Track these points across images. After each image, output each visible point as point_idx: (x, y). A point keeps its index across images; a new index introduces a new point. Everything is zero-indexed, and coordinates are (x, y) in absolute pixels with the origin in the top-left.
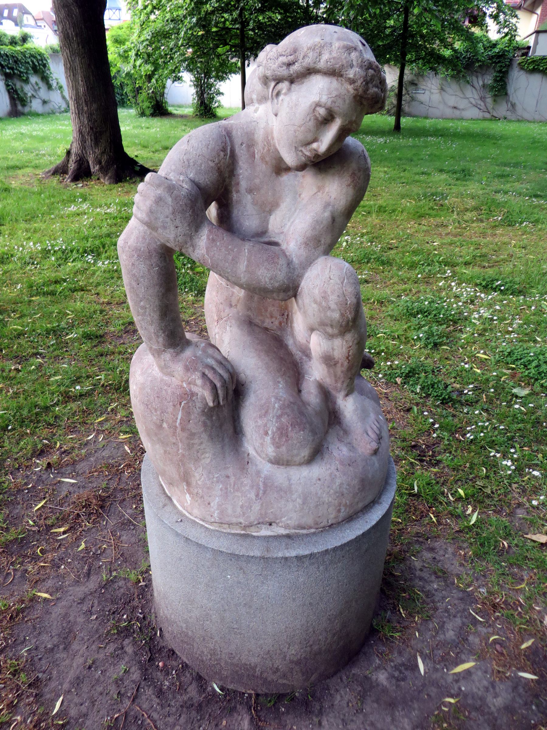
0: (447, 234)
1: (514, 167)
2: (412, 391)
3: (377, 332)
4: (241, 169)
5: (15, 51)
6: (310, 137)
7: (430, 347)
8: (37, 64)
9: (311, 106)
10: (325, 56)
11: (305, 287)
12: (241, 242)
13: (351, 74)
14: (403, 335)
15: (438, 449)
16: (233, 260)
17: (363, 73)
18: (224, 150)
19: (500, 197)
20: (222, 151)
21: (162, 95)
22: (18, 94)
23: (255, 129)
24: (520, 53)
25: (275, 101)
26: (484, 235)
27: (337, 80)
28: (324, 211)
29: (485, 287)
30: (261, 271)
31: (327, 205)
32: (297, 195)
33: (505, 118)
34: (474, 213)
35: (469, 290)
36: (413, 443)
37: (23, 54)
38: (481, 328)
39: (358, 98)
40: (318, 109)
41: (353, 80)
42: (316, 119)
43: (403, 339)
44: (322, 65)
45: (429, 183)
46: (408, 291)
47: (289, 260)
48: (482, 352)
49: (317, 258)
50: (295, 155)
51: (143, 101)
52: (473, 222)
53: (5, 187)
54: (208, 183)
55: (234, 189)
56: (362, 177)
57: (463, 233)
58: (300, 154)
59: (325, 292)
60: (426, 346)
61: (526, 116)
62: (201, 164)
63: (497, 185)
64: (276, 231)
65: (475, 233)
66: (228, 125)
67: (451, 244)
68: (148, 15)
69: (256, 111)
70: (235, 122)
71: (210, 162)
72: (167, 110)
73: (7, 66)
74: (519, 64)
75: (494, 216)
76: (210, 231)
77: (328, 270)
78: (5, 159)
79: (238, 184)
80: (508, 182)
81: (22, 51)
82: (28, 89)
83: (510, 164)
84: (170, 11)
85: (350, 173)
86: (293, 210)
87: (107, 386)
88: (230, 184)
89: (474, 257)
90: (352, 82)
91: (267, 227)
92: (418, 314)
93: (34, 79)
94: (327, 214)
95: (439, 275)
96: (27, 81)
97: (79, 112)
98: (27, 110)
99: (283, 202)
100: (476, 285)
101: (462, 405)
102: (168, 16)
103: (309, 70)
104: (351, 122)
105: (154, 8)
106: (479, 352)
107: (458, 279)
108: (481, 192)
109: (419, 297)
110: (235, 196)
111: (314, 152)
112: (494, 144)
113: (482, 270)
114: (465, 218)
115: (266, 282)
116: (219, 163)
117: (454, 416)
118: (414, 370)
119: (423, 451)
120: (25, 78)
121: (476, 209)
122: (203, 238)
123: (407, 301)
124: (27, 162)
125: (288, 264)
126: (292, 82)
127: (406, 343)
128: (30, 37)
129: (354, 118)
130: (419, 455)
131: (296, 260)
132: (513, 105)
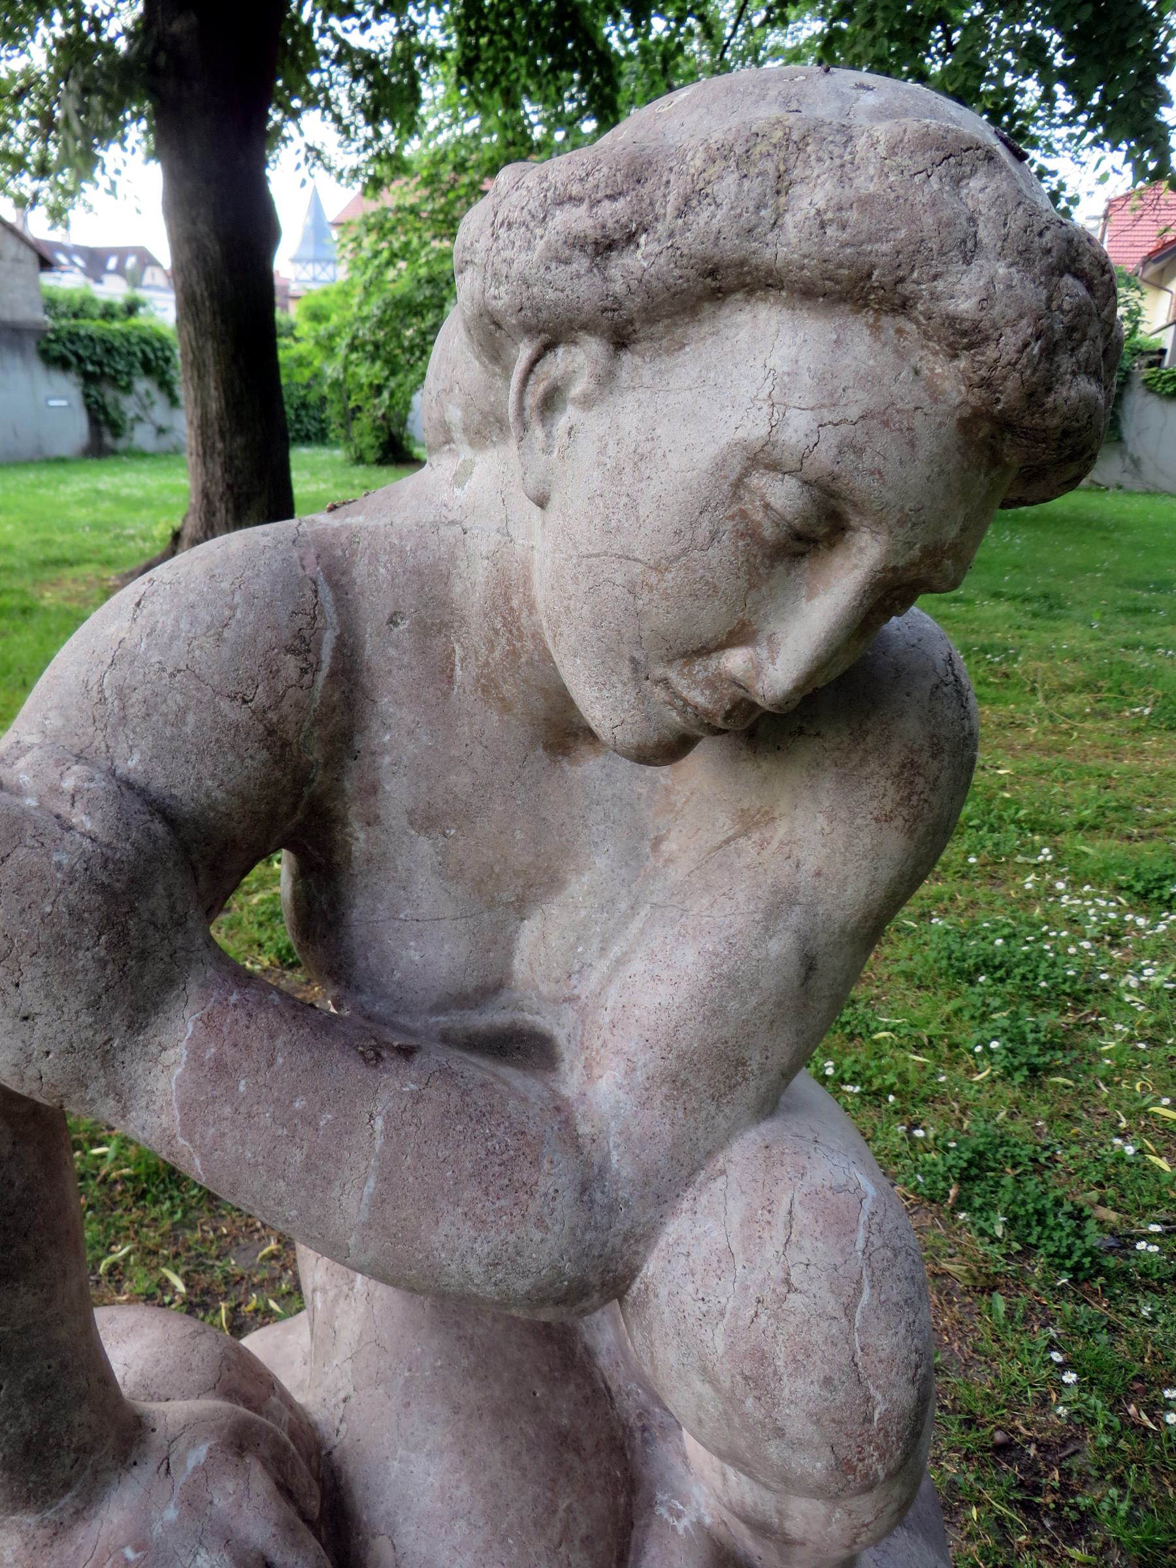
0: (1028, 747)
1: (1157, 590)
2: (982, 1233)
3: (873, 1025)
4: (387, 727)
5: (110, 331)
6: (710, 620)
7: (1019, 1078)
8: (152, 356)
9: (720, 465)
10: (813, 195)
11: (663, 1292)
12: (359, 1071)
13: (963, 293)
14: (942, 1037)
15: (1076, 1463)
16: (309, 1166)
17: (1032, 294)
18: (303, 646)
19: (1139, 660)
20: (290, 650)
21: (403, 422)
22: (106, 413)
23: (453, 558)
24: (1144, 362)
25: (538, 432)
26: (1116, 753)
27: (875, 329)
28: (768, 932)
29: (1144, 895)
30: (445, 1228)
31: (781, 901)
32: (640, 846)
33: (1120, 487)
34: (1086, 697)
35: (1103, 903)
36: (999, 1436)
37: (126, 337)
38: (1151, 1020)
39: (985, 429)
40: (757, 480)
41: (976, 327)
42: (750, 533)
43: (943, 1047)
44: (789, 243)
45: (971, 621)
46: (946, 902)
47: (588, 1164)
48: (1166, 1101)
49: (722, 1144)
50: (631, 696)
51: (361, 435)
52: (1085, 717)
53: (27, 603)
54: (219, 794)
55: (354, 812)
56: (944, 777)
57: (1065, 745)
58: (660, 694)
59: (761, 1357)
60: (1009, 1072)
61: (1164, 483)
62: (183, 711)
63: (1125, 629)
64: (544, 989)
65: (1094, 746)
66: (337, 532)
67: (1039, 774)
68: (381, 270)
69: (460, 477)
70: (371, 524)
71: (225, 705)
72: (410, 453)
73: (90, 358)
74: (1145, 381)
75: (1131, 705)
76: (208, 1022)
77: (780, 1234)
78: (47, 542)
79: (373, 789)
80: (1149, 624)
81: (125, 330)
82: (129, 406)
83: (1147, 584)
84: (428, 262)
85: (896, 760)
86: (623, 906)
87: (115, 1182)
88: (335, 790)
89: (1102, 811)
90: (965, 337)
91: (508, 965)
92: (977, 970)
93: (143, 385)
94: (780, 946)
95: (1020, 859)
96: (128, 389)
97: (206, 452)
98: (121, 444)
99: (579, 872)
100: (1119, 889)
101: (1133, 1287)
102: (423, 272)
103: (712, 273)
104: (933, 554)
105: (394, 255)
106: (1156, 1102)
107: (1068, 873)
108: (1092, 646)
109: (974, 923)
110: (360, 839)
111: (729, 691)
112: (1104, 539)
113: (1125, 844)
114: (1066, 707)
115: (469, 1277)
116: (276, 706)
117: (1113, 1329)
118: (981, 1155)
119: (1030, 1468)
120: (123, 383)
121: (1088, 686)
122: (169, 1056)
123: (947, 932)
124: (89, 551)
125: (584, 1188)
126: (621, 340)
127: (954, 1061)
128: (144, 305)
129: (952, 532)
130: (1021, 1485)
131: (621, 1164)
132: (1136, 462)
